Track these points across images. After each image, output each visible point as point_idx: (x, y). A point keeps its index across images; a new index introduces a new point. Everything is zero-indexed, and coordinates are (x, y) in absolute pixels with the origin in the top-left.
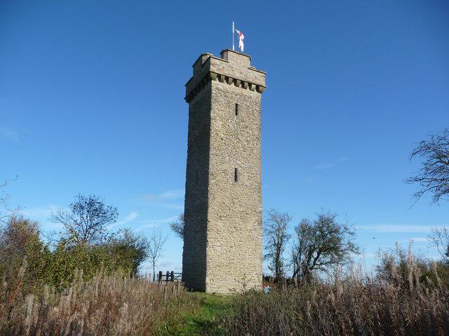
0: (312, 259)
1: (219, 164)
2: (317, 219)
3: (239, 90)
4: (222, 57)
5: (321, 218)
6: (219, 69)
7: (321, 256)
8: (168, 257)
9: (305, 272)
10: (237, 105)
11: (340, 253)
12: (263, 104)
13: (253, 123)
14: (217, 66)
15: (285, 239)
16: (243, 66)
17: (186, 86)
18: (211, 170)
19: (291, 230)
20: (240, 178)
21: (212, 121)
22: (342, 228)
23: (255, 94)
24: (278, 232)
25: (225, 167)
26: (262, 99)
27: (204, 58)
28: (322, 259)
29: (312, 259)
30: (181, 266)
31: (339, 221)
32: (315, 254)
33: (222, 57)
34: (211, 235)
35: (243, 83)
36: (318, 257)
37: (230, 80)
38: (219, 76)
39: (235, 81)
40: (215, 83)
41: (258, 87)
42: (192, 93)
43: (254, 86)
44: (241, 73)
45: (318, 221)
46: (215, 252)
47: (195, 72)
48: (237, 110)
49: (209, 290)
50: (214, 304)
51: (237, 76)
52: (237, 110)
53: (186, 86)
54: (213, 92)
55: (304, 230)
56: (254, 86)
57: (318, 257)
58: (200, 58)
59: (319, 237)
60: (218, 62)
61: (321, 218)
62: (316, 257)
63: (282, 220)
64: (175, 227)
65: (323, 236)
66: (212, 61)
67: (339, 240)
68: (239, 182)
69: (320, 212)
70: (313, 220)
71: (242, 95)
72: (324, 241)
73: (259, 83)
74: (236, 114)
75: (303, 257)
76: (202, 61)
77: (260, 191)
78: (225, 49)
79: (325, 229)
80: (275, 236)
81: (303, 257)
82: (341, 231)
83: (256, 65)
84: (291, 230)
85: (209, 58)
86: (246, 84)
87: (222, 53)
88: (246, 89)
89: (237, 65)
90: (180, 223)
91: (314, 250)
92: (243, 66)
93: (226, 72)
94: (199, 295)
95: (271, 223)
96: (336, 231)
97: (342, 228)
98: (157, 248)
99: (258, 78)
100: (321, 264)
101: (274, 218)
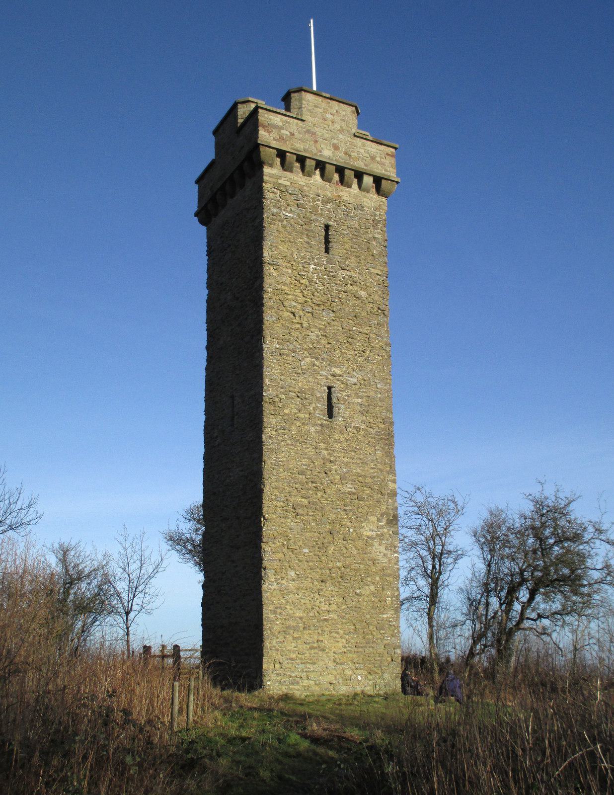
0: (517, 607)
1: (287, 373)
2: (528, 508)
3: (331, 189)
4: (288, 108)
5: (539, 504)
6: (282, 139)
7: (538, 598)
8: (171, 609)
9: (497, 634)
10: (327, 227)
11: (585, 590)
12: (392, 221)
13: (366, 277)
14: (276, 129)
15: (450, 560)
16: (341, 131)
17: (197, 182)
18: (269, 392)
19: (462, 538)
20: (340, 409)
21: (268, 270)
22: (591, 529)
23: (372, 201)
24: (431, 543)
25: (302, 383)
26: (389, 205)
27: (243, 112)
28: (542, 606)
29: (517, 607)
30: (200, 630)
31: (582, 513)
32: (523, 594)
33: (288, 108)
34: (271, 552)
35: (340, 170)
36: (531, 599)
37: (310, 164)
38: (281, 154)
39: (321, 165)
40: (271, 172)
41: (378, 180)
42: (213, 199)
43: (368, 180)
44: (336, 147)
45: (528, 514)
46: (285, 591)
47: (219, 147)
48: (327, 241)
49: (275, 682)
50: (292, 712)
51: (327, 154)
52: (327, 241)
53: (197, 182)
54: (268, 195)
55: (492, 537)
56: (368, 180)
57: (531, 599)
58: (234, 108)
59: (535, 552)
60: (277, 120)
61: (539, 504)
62: (525, 599)
63: (440, 513)
64: (176, 540)
65: (544, 549)
66: (263, 116)
67: (582, 557)
68: (339, 420)
69: (536, 491)
70: (517, 508)
71: (338, 202)
72: (232, 692)
73: (379, 170)
74: (327, 250)
75: (494, 602)
76: (236, 117)
77: (388, 440)
78: (294, 87)
79: (548, 532)
80: (424, 553)
81: (494, 602)
82: (587, 537)
83: (372, 126)
84: (462, 538)
85: (257, 108)
86: (349, 174)
87: (287, 100)
88: (350, 186)
89: (322, 125)
90: (191, 530)
91: (520, 584)
92: (341, 131)
93: (299, 146)
94: (244, 698)
95: (419, 520)
96: (576, 538)
97: (591, 529)
98: (134, 590)
99: (377, 158)
100: (540, 616)
101: (422, 509)
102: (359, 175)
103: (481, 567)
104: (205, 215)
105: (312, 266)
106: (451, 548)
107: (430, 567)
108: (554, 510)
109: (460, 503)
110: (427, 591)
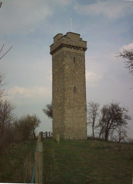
2: (110, 105)
3: (75, 51)
5: (112, 105)
10: (74, 58)
17: (54, 38)
31: (120, 106)
39: (73, 46)
44: (76, 43)
53: (53, 38)
55: (104, 111)
56: (82, 49)
61: (112, 105)
67: (121, 114)
100: (113, 126)
102: (80, 48)
103: (102, 117)
104: (52, 53)
105: (76, 126)
106: (97, 113)
107: (93, 117)
108: (116, 106)
109: (99, 104)
110: (92, 121)
